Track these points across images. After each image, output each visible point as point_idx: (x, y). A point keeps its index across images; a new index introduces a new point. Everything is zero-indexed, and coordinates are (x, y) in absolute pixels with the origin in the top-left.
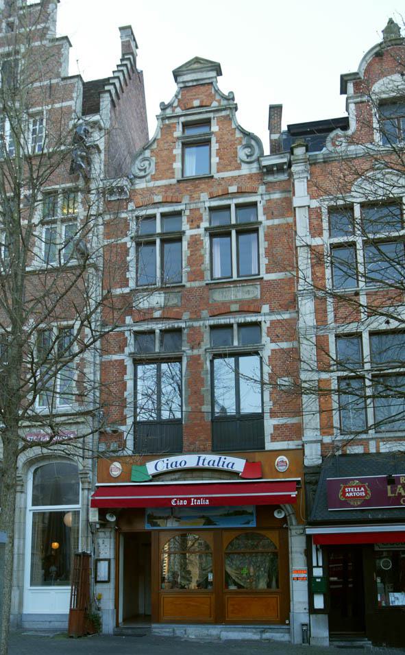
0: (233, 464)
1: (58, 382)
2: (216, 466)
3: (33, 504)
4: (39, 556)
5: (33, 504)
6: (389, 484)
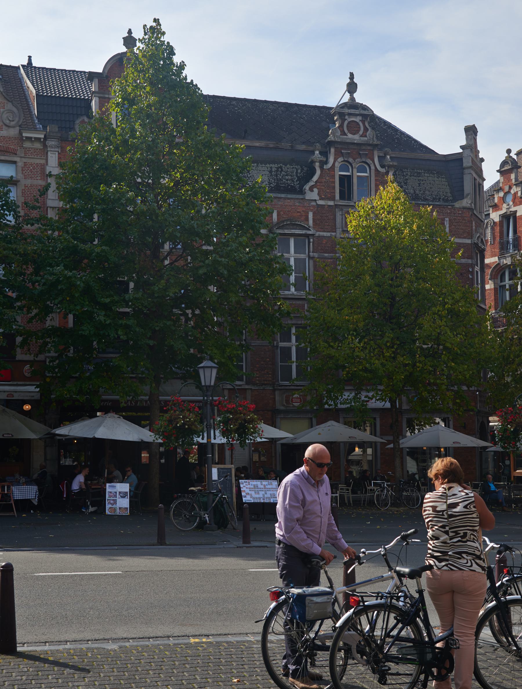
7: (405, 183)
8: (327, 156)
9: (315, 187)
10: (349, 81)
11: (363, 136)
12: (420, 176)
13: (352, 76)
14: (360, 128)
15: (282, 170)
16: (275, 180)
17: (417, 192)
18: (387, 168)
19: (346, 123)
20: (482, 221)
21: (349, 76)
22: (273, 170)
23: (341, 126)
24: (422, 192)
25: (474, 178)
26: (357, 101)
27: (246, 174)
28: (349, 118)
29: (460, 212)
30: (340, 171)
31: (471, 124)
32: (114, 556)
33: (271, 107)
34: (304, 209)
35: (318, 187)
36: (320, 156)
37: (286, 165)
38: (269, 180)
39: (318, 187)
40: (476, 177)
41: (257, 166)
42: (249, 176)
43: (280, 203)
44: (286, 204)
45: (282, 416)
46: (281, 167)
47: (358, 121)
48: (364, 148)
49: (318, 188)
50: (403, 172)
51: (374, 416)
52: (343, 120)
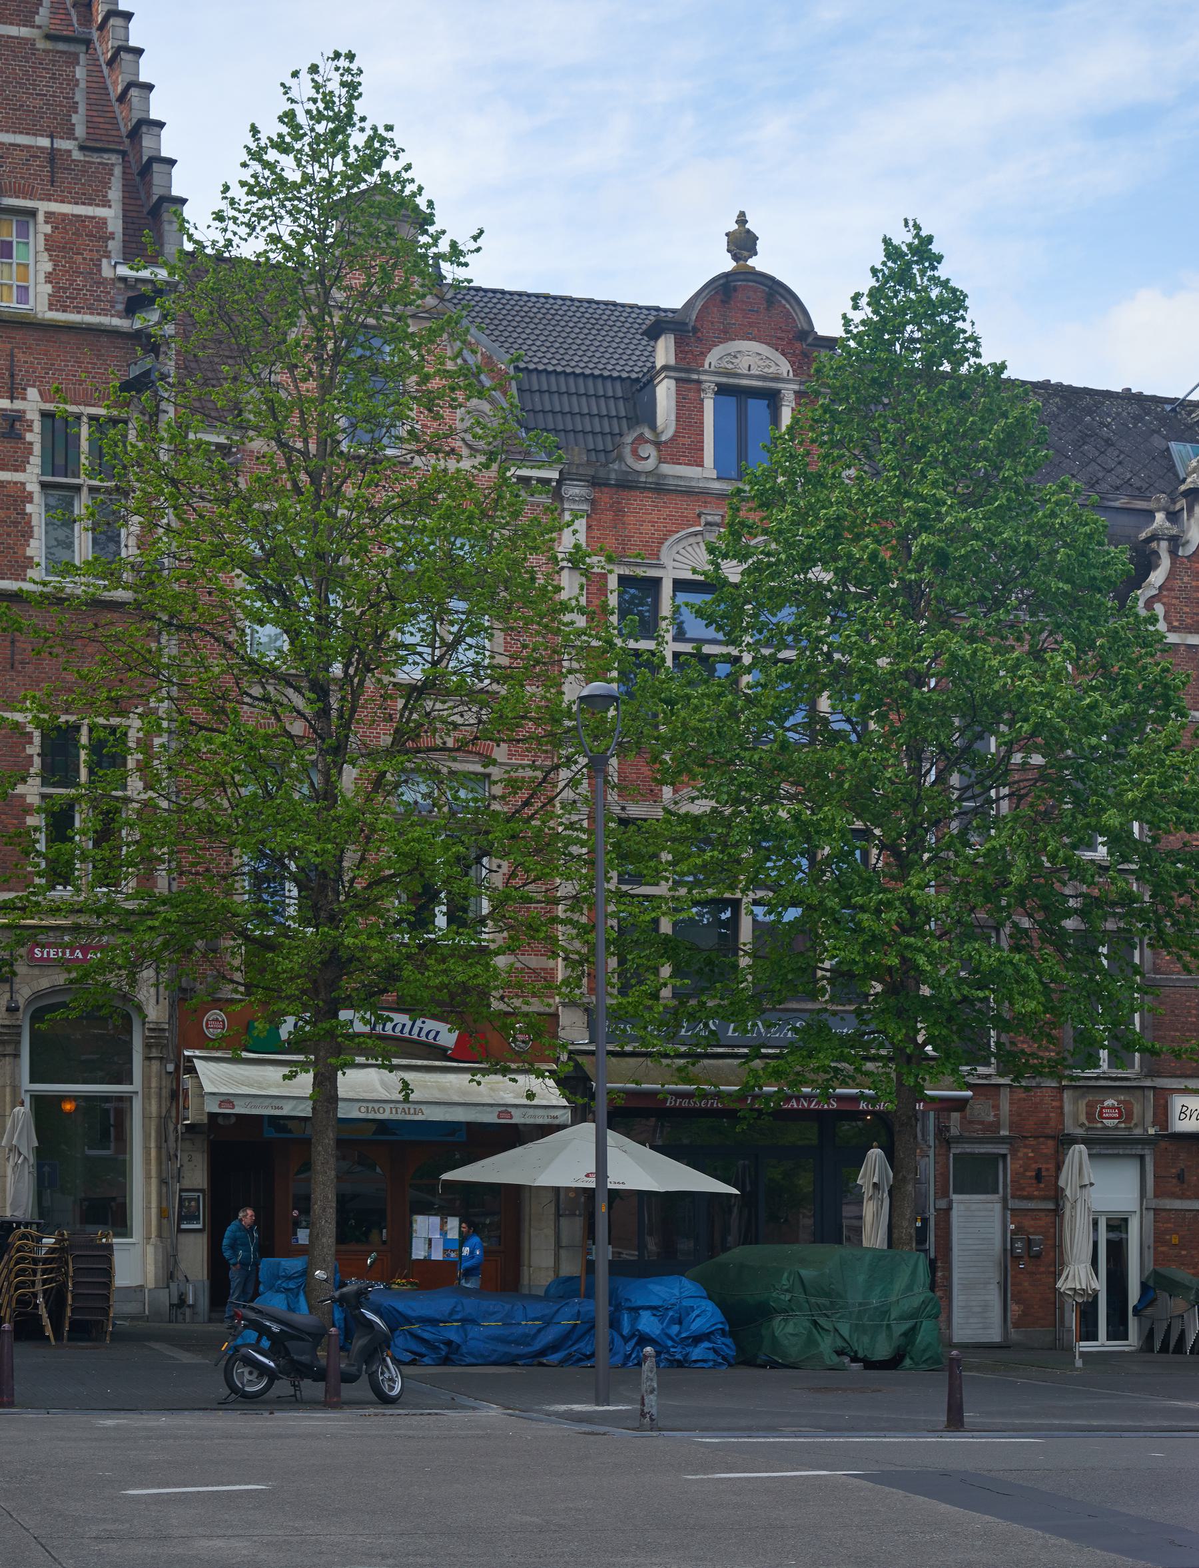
0: (438, 1033)
1: (905, 765)
2: (407, 1035)
3: (33, 1080)
4: (36, 1209)
5: (33, 1080)
6: (336, 1016)
9: (1159, 601)
39: (1165, 600)
49: (1163, 604)
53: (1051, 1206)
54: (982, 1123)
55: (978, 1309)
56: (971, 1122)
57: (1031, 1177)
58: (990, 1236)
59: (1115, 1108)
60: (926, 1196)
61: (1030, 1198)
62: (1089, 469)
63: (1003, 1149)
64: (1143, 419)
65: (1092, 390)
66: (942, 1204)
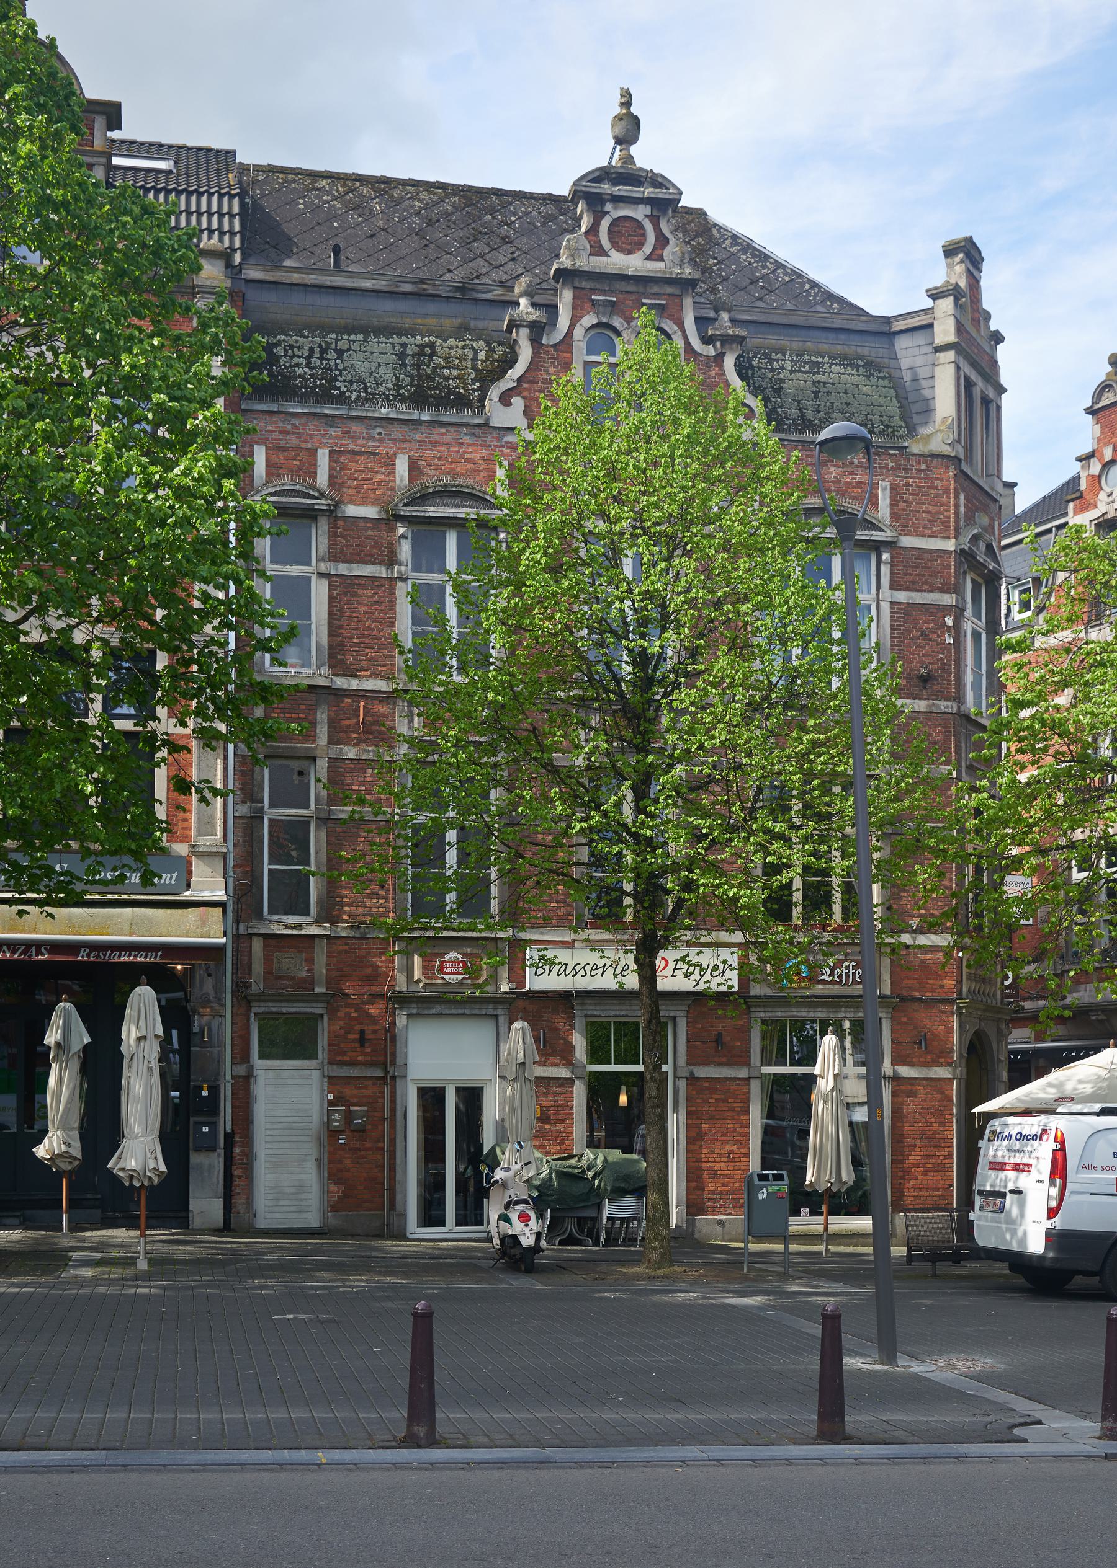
7: (775, 391)
8: (552, 310)
9: (518, 395)
10: (617, 110)
11: (655, 256)
12: (818, 373)
13: (627, 103)
14: (644, 235)
15: (434, 353)
16: (412, 377)
17: (809, 414)
18: (718, 344)
19: (605, 224)
20: (995, 500)
21: (617, 99)
22: (409, 352)
23: (593, 230)
24: (821, 415)
25: (967, 379)
26: (638, 165)
27: (332, 363)
28: (615, 208)
29: (923, 467)
30: (588, 353)
31: (968, 235)
32: (683, 1159)
33: (425, 196)
34: (485, 454)
35: (525, 393)
36: (531, 309)
37: (445, 341)
38: (397, 378)
39: (525, 393)
40: (974, 376)
41: (365, 341)
42: (341, 367)
43: (417, 437)
44: (436, 438)
45: (415, 1011)
46: (432, 345)
47: (640, 217)
48: (655, 289)
49: (524, 398)
50: (771, 361)
51: (672, 1014)
52: (599, 216)
53: (379, 1073)
54: (293, 978)
55: (292, 1190)
56: (279, 978)
57: (354, 1041)
58: (307, 1107)
59: (459, 963)
60: (220, 1060)
61: (352, 1064)
62: (473, 264)
63: (318, 1009)
64: (556, 218)
65: (501, 190)
66: (241, 1070)
